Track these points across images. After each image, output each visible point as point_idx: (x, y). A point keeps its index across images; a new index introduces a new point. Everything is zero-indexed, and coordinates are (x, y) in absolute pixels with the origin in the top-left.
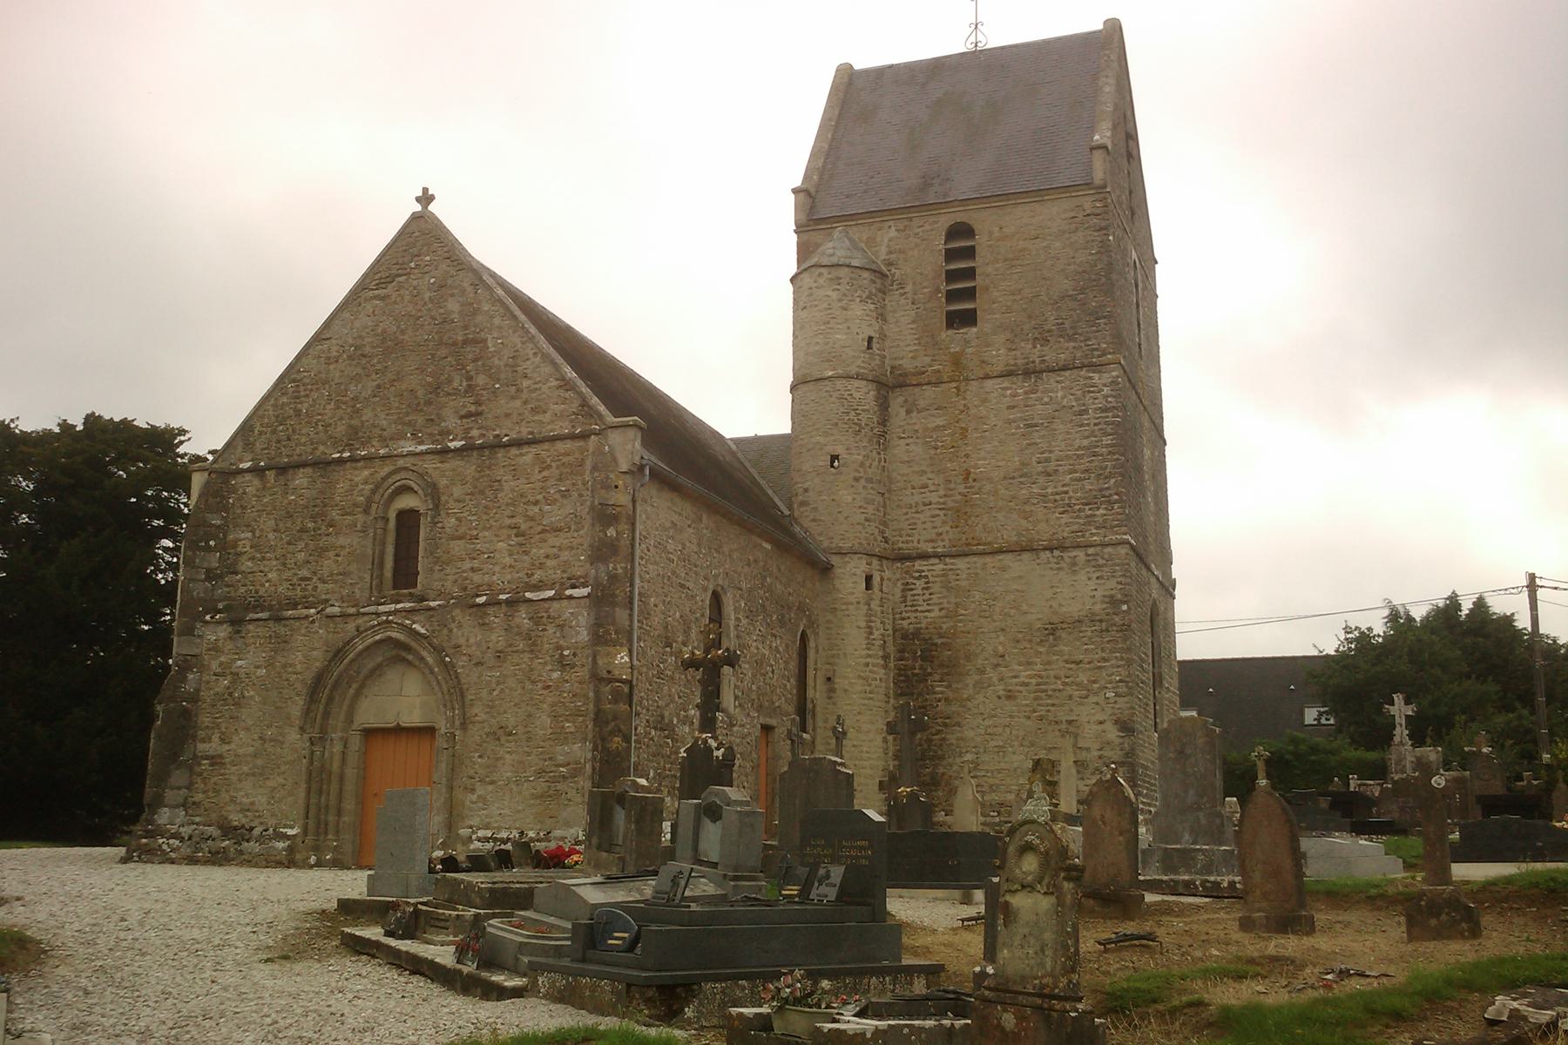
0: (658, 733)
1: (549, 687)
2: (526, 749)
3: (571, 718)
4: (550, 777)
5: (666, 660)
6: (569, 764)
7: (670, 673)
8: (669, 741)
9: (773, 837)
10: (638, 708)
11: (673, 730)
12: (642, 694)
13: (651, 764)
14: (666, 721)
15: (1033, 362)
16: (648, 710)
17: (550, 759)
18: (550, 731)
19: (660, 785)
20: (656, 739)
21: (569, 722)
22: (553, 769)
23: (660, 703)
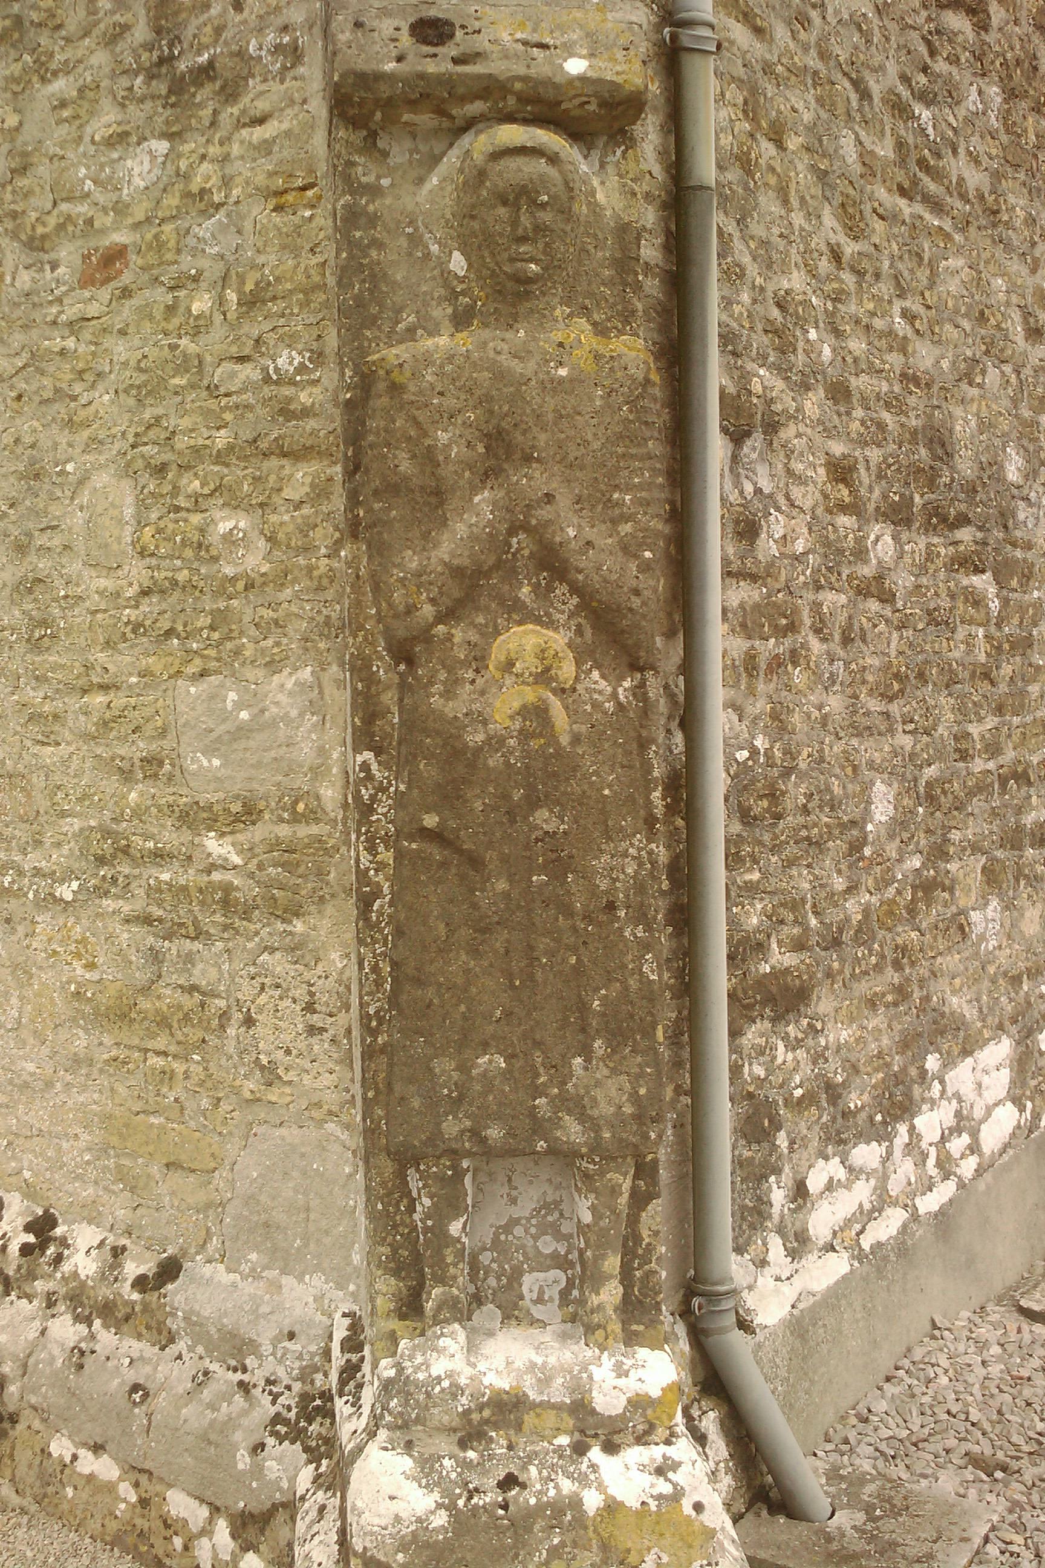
0: (918, 544)
1: (114, 257)
2: (34, 695)
3: (236, 473)
4: (155, 892)
5: (954, 97)
6: (250, 813)
7: (975, 179)
8: (983, 582)
9: (341, 76)
10: (763, 379)
11: (1005, 519)
12: (796, 281)
13: (869, 750)
14: (966, 467)
15: (793, 1045)
16: (839, 393)
17: (152, 762)
18: (137, 572)
19: (939, 852)
20: (902, 581)
21: (235, 504)
22: (171, 837)
23: (924, 356)
